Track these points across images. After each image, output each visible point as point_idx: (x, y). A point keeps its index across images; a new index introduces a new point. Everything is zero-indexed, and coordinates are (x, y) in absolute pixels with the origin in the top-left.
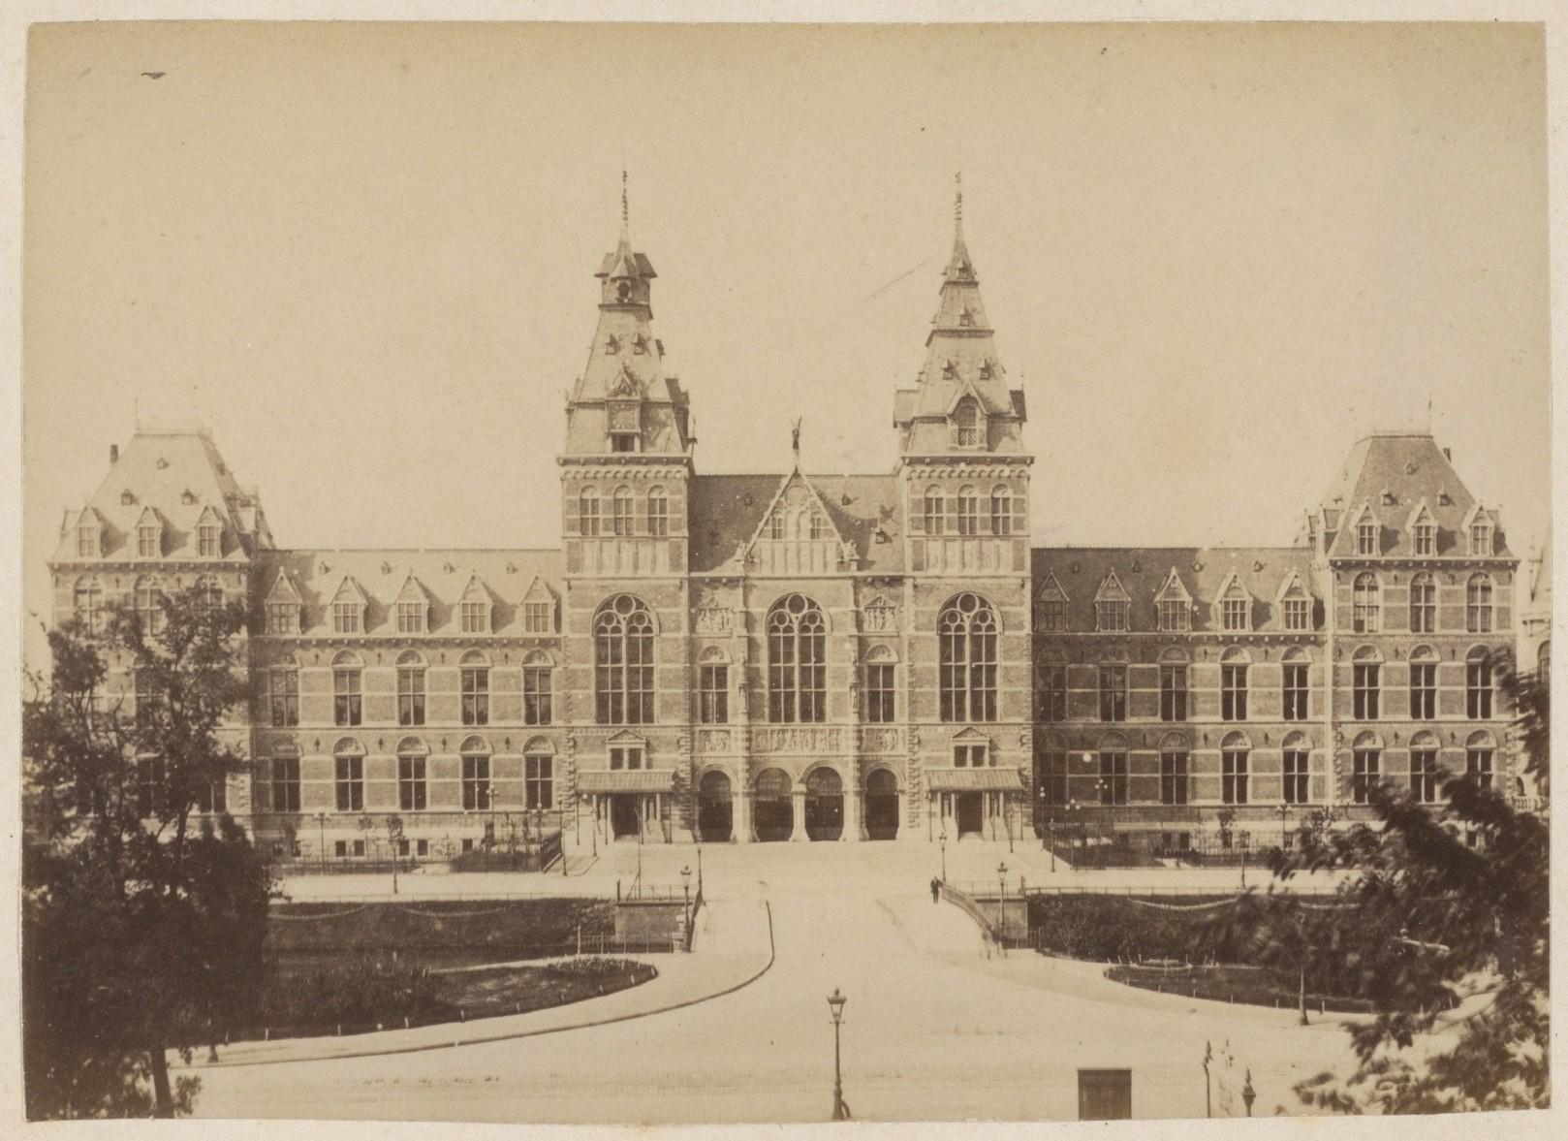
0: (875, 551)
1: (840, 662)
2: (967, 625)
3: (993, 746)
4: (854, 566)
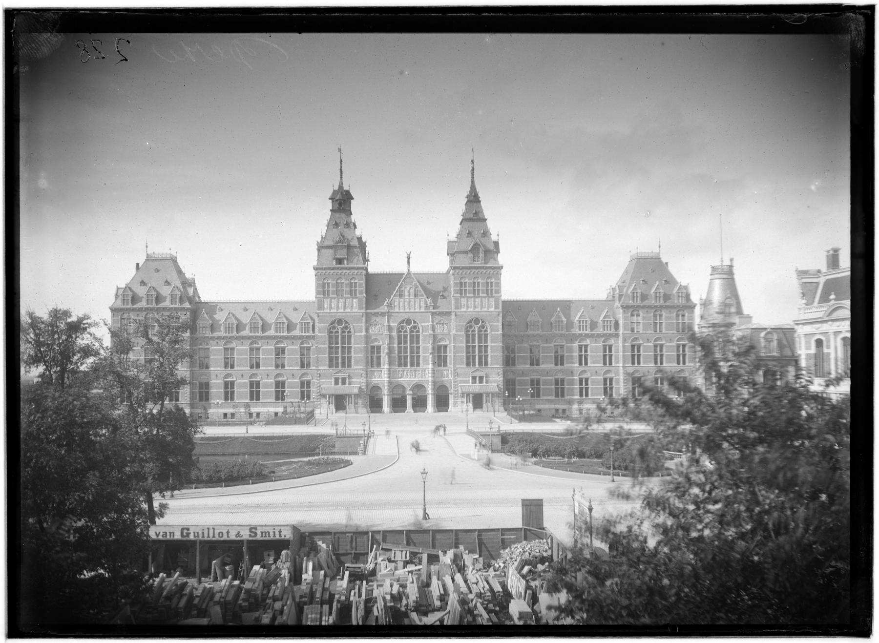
0: (440, 302)
1: (426, 347)
3: (487, 376)
4: (432, 308)
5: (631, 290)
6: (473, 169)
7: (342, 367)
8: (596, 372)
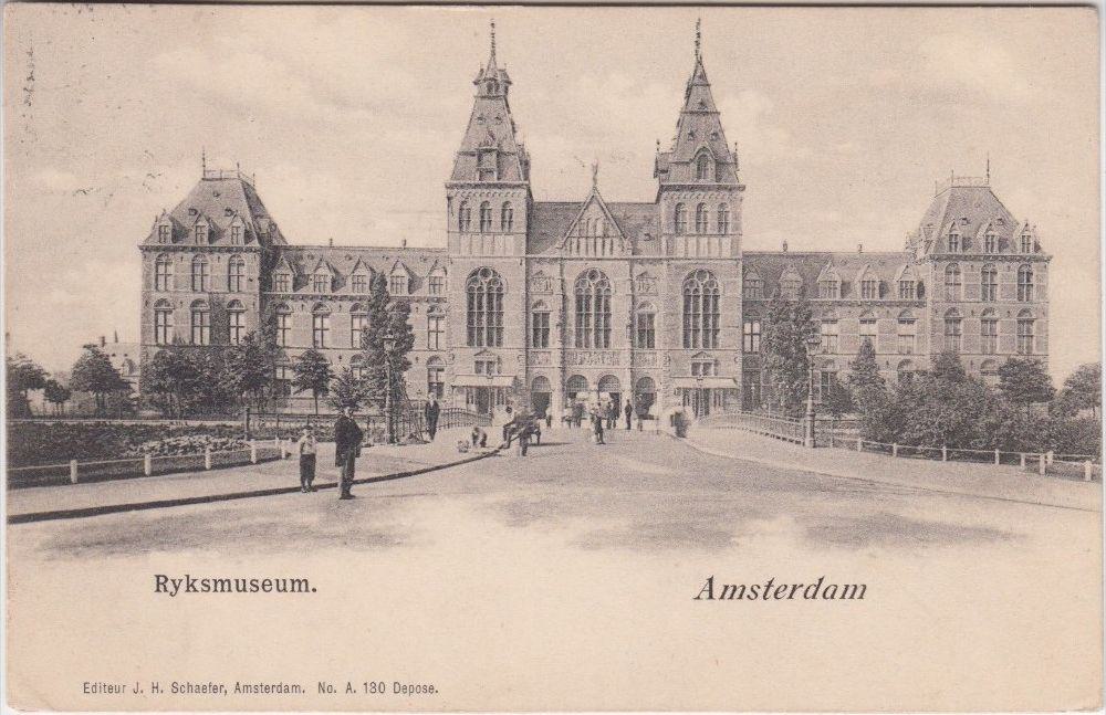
2: (485, 287)
5: (946, 231)
6: (399, 688)
7: (488, 345)
8: (888, 363)
